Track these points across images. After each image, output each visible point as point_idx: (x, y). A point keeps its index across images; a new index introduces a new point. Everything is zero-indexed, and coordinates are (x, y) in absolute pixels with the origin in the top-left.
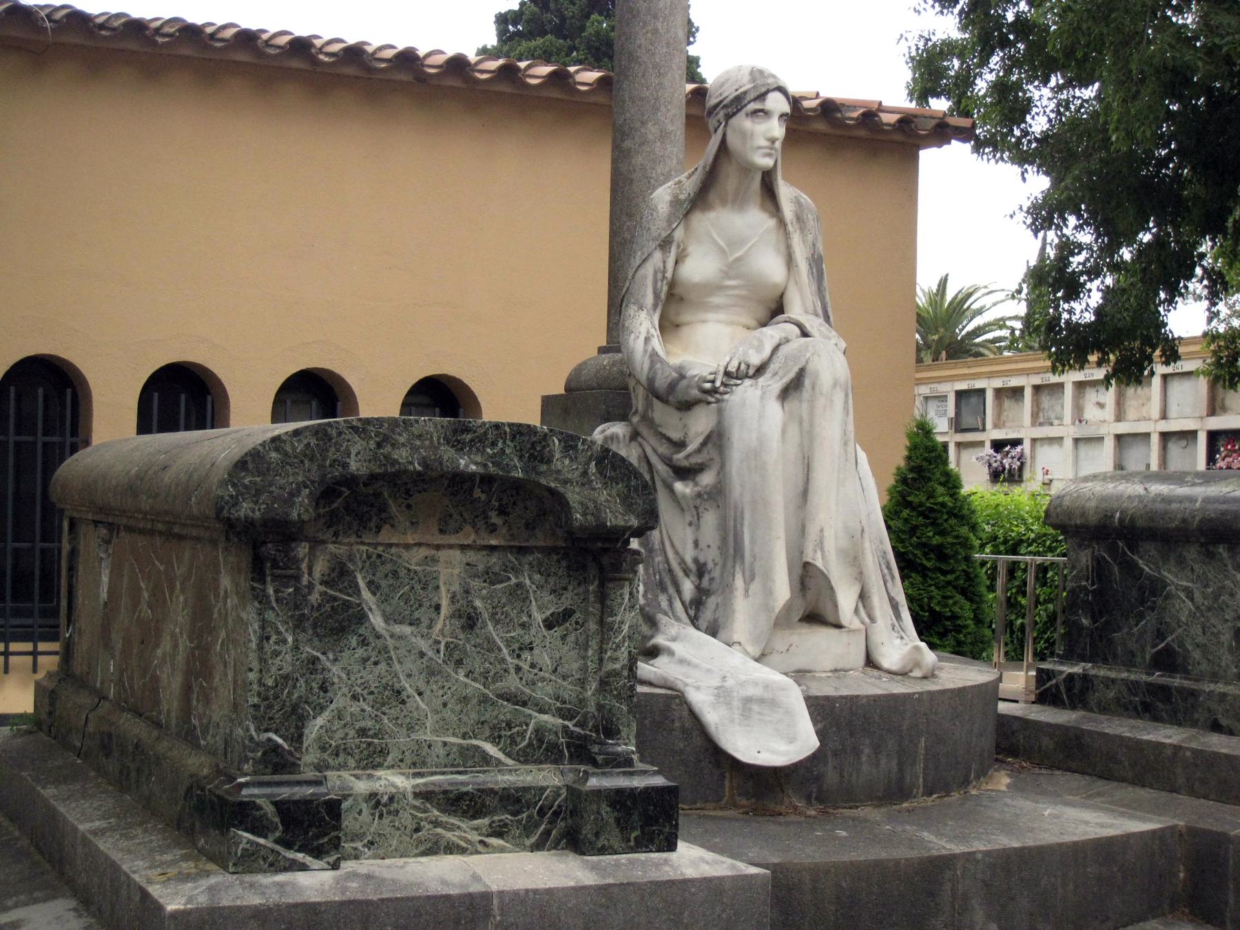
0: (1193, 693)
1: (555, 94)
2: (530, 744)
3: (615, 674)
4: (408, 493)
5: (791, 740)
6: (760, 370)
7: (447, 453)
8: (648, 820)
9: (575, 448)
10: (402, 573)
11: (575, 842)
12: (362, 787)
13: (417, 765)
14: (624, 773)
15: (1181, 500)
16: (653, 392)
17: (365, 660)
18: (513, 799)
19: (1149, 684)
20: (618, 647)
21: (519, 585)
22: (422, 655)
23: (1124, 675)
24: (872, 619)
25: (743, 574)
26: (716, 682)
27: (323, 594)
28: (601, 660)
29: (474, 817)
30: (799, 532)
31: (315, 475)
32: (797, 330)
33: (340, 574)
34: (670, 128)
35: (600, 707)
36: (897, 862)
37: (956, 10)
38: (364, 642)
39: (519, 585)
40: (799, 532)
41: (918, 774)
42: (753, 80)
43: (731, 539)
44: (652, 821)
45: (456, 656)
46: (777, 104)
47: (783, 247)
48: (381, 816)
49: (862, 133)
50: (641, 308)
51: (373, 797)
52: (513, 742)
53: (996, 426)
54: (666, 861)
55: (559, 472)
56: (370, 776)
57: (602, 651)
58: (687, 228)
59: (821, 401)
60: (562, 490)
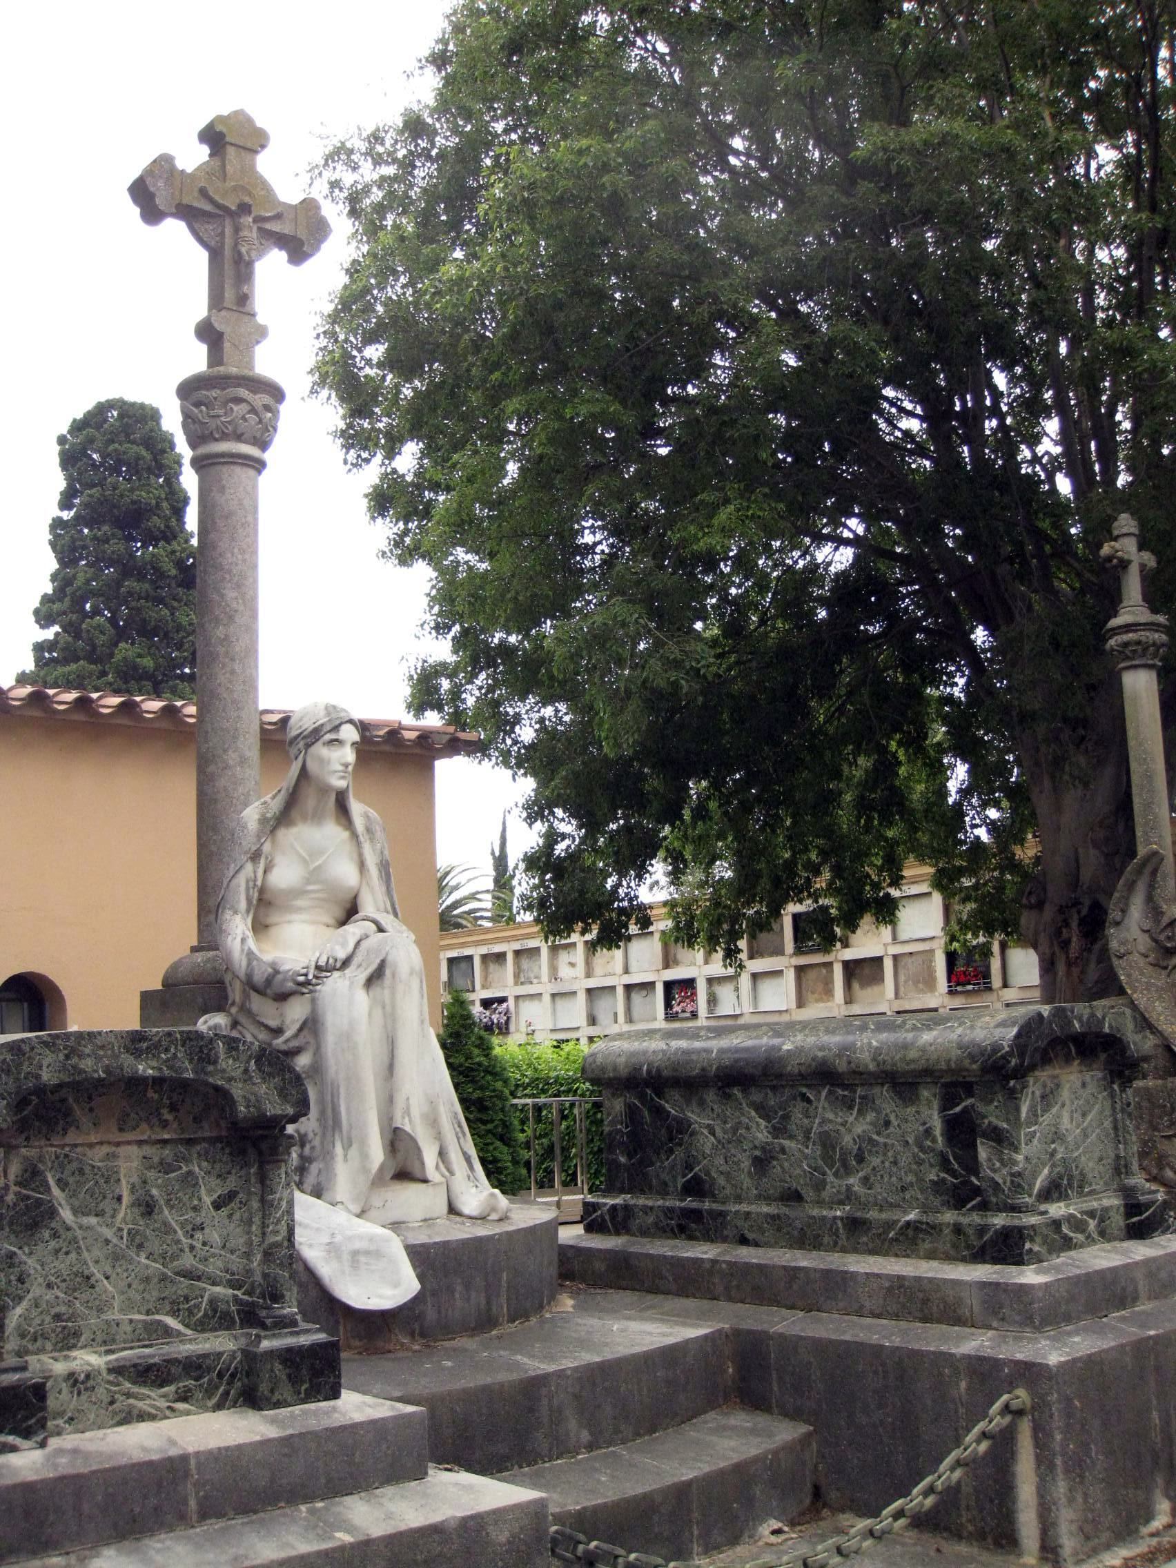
0: (722, 1214)
1: (124, 721)
2: (205, 1315)
3: (277, 1245)
5: (396, 1285)
6: (346, 963)
8: (316, 1373)
9: (237, 1049)
10: (87, 1169)
11: (252, 1399)
12: (60, 1368)
13: (107, 1343)
14: (292, 1334)
15: (699, 1051)
16: (250, 985)
17: (57, 1251)
18: (194, 1366)
19: (682, 1210)
20: (279, 1221)
21: (190, 1173)
22: (107, 1242)
23: (660, 1203)
24: (452, 1173)
26: (326, 1240)
27: (16, 1194)
28: (264, 1234)
29: (161, 1386)
30: (389, 1100)
32: (374, 927)
33: (32, 1175)
34: (248, 754)
35: (265, 1276)
36: (502, 1385)
37: (450, 636)
38: (55, 1235)
39: (190, 1173)
40: (389, 1100)
41: (502, 1306)
42: (328, 714)
43: (329, 1112)
44: (317, 1374)
45: (138, 1240)
46: (350, 734)
47: (355, 856)
48: (79, 1394)
49: (387, 748)
50: (236, 913)
51: (71, 1377)
52: (191, 1313)
53: (484, 987)
54: (334, 1409)
55: (224, 1071)
56: (66, 1358)
57: (264, 1226)
58: (273, 842)
59: (400, 988)
60: (227, 1086)
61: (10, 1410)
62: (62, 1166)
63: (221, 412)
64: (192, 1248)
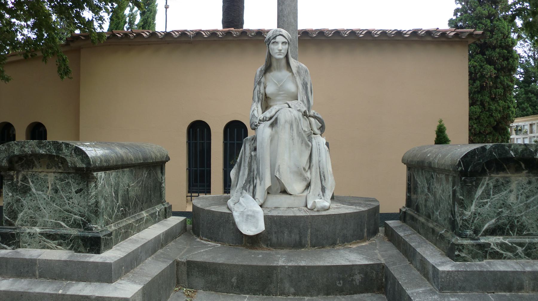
2: (73, 223)
4: (39, 159)
5: (256, 228)
7: (37, 149)
9: (68, 147)
10: (39, 179)
13: (45, 225)
18: (64, 237)
22: (45, 199)
29: (54, 240)
31: (7, 155)
38: (31, 195)
39: (68, 182)
58: (265, 78)
61: (11, 240)
62: (32, 177)
64: (69, 204)
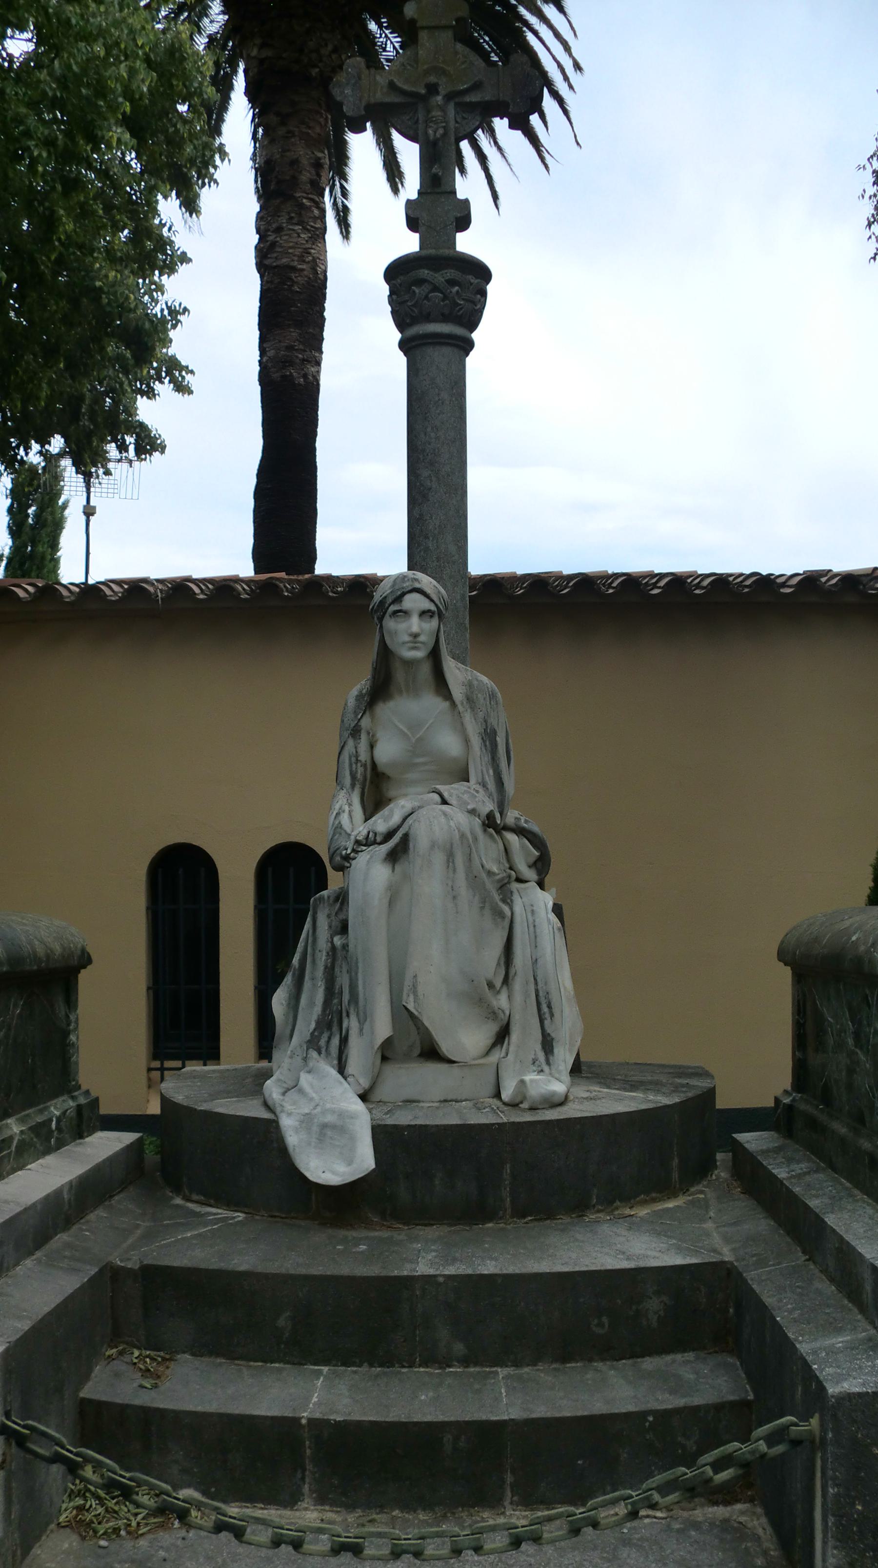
5: (350, 1163)
25: (358, 1015)
58: (373, 717)
63: (407, 297)
